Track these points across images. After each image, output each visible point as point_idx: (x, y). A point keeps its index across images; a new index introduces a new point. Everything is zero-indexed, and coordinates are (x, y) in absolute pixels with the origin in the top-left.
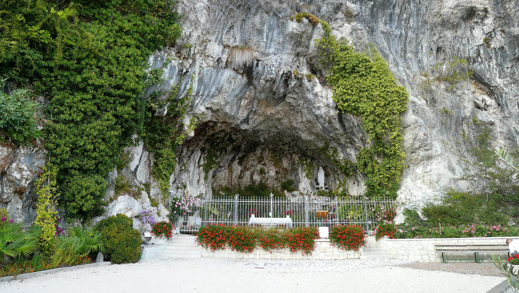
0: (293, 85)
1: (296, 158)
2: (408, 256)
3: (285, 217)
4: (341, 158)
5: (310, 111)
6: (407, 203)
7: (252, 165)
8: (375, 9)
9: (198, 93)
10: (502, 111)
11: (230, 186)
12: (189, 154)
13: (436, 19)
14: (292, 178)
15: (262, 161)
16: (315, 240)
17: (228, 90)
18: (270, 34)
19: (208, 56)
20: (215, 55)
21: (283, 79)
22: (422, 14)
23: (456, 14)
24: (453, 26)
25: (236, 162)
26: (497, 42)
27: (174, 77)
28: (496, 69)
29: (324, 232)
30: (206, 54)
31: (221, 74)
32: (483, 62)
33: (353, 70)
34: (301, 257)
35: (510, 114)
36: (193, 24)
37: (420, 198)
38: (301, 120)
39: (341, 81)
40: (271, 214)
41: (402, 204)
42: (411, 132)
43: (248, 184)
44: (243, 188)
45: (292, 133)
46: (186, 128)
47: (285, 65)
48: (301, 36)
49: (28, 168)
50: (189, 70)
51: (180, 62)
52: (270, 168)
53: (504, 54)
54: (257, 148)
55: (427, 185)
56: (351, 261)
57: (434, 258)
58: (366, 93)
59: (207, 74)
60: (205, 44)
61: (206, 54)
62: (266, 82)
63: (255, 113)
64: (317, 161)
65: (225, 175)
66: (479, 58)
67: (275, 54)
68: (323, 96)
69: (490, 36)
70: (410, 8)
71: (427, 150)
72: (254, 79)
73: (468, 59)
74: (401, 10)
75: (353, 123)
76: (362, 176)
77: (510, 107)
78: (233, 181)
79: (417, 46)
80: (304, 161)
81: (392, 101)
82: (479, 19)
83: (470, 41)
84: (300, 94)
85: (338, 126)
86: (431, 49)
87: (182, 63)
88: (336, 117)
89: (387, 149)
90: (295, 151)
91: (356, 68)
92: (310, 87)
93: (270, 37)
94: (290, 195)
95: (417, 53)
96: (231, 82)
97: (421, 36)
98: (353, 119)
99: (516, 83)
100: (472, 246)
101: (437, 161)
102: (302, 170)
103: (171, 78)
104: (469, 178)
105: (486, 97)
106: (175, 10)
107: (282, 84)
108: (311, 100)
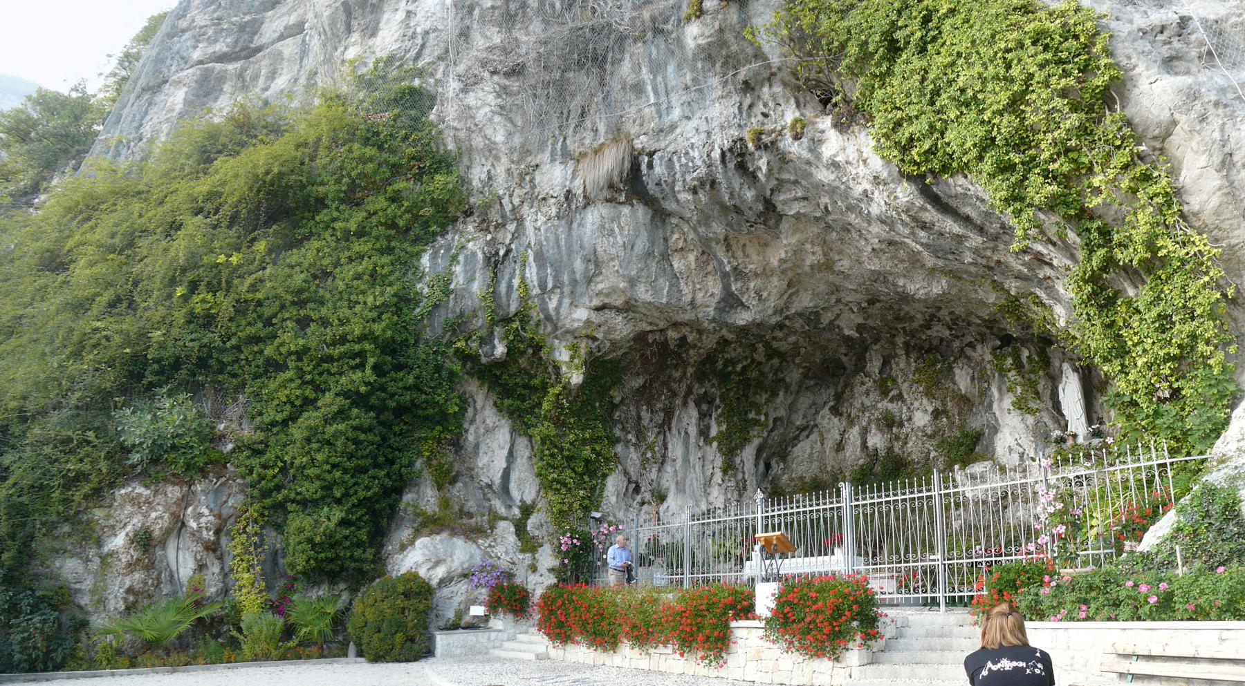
3: (833, 554)
9: (543, 286)
12: (660, 417)
16: (733, 624)
17: (613, 251)
19: (544, 199)
21: (731, 165)
27: (478, 275)
31: (580, 225)
33: (893, 49)
38: (869, 249)
42: (1194, 144)
48: (722, 43)
49: (211, 511)
50: (513, 246)
51: (489, 237)
52: (916, 404)
59: (547, 239)
60: (528, 178)
67: (688, 118)
72: (662, 202)
87: (493, 239)
88: (919, 202)
92: (806, 154)
93: (661, 88)
96: (612, 230)
102: (1000, 390)
103: (471, 280)
106: (442, 148)
107: (737, 181)
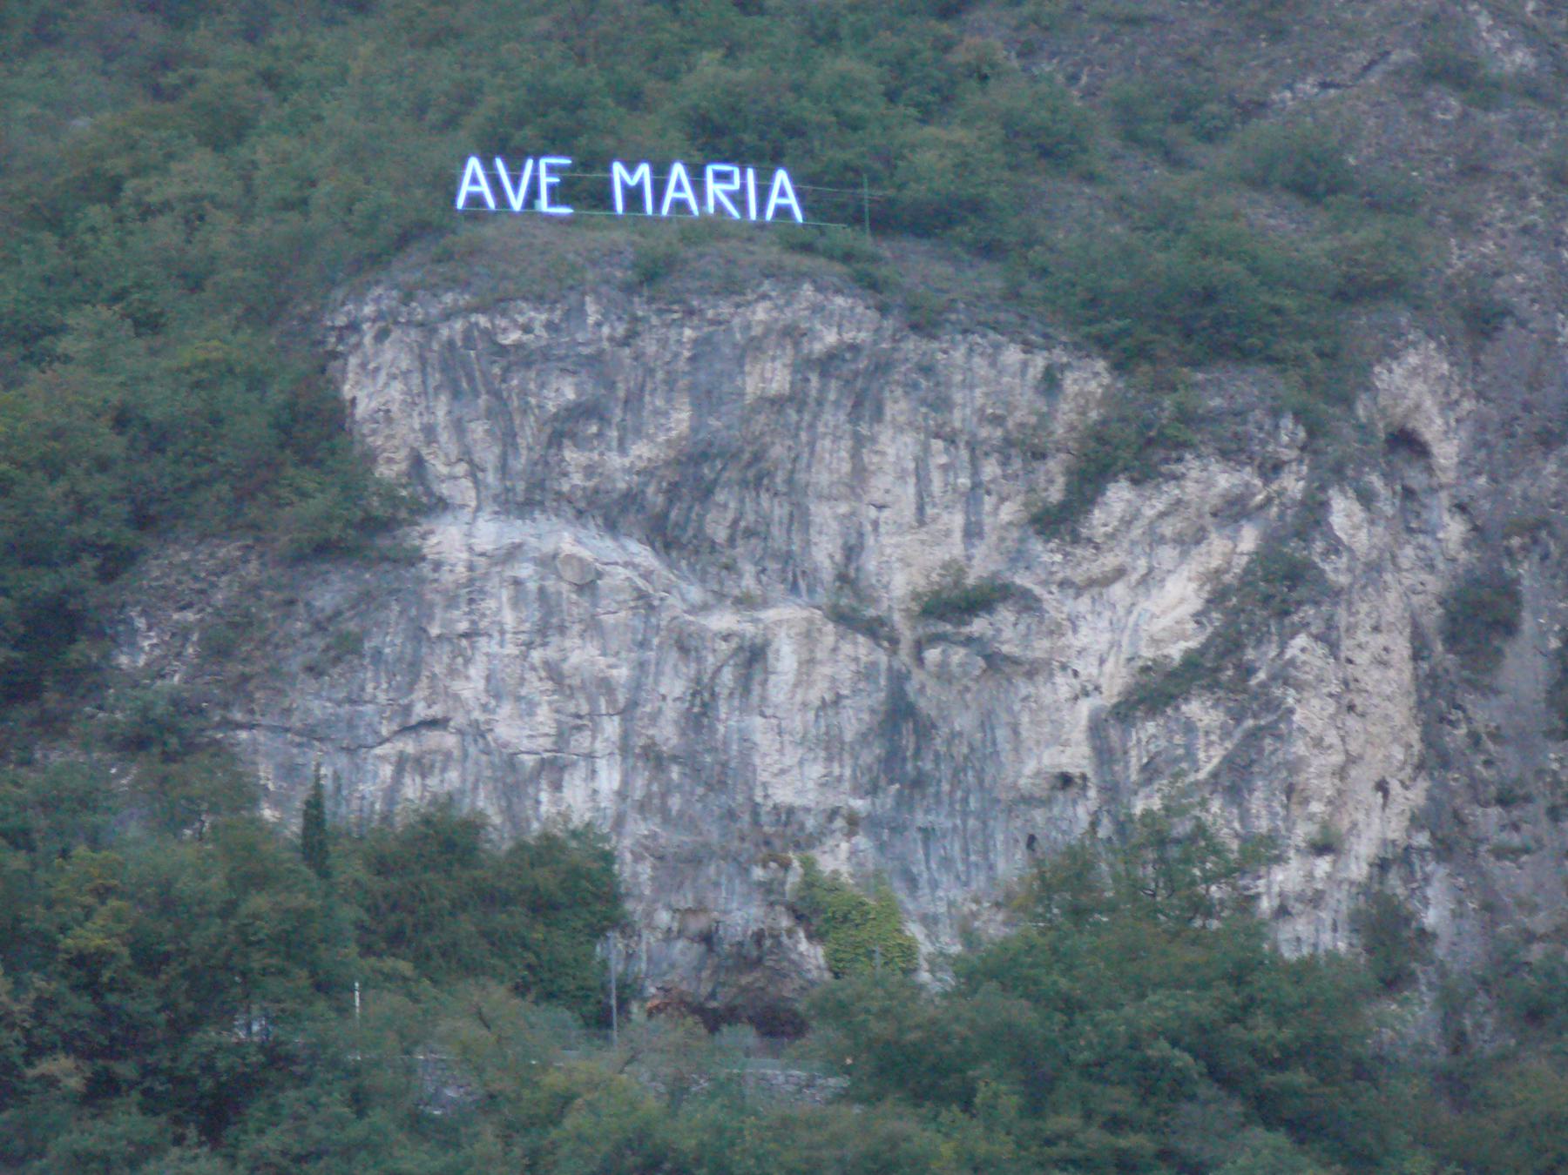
33: (845, 919)
39: (832, 935)
63: (723, 984)
79: (985, 843)
97: (991, 823)
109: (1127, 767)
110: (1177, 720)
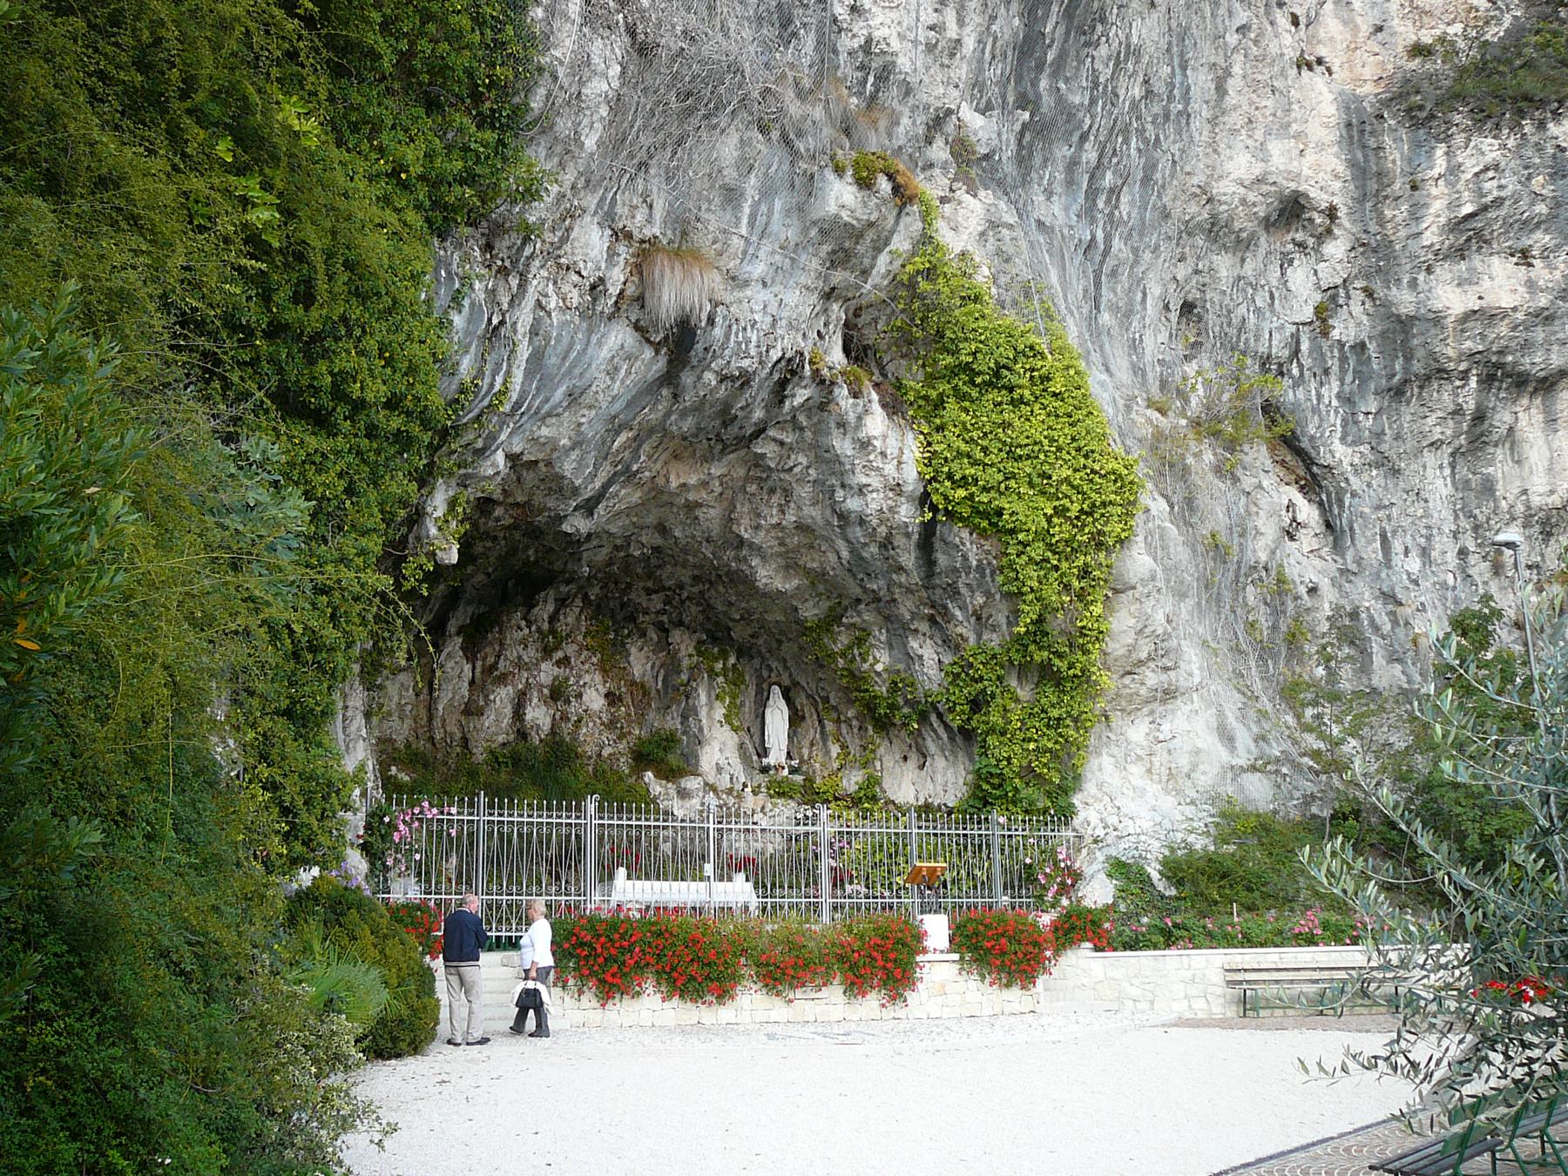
0: (798, 401)
1: (684, 645)
2: (1152, 1002)
3: (730, 879)
4: (879, 667)
5: (825, 493)
6: (1110, 840)
7: (520, 664)
8: (1028, 137)
10: (1337, 547)
11: (422, 745)
13: (1193, 209)
14: (673, 722)
15: (557, 648)
16: (919, 958)
18: (763, 208)
20: (590, 264)
21: (776, 376)
22: (1160, 182)
23: (1254, 205)
24: (1239, 241)
25: (455, 644)
26: (1351, 324)
28: (1336, 412)
29: (937, 928)
30: (563, 260)
32: (1304, 382)
34: (876, 1014)
35: (1359, 564)
36: (558, 149)
37: (1147, 825)
40: (709, 869)
41: (1096, 841)
42: (1133, 608)
43: (501, 739)
44: (479, 754)
45: (719, 558)
46: (433, 531)
47: (790, 326)
48: (858, 236)
52: (587, 678)
53: (1364, 369)
54: (543, 594)
55: (1160, 782)
56: (1012, 1019)
57: (1219, 1003)
58: (1027, 467)
61: (563, 260)
62: (721, 381)
64: (757, 662)
65: (401, 696)
66: (1295, 365)
68: (889, 452)
69: (1334, 298)
70: (1129, 155)
71: (1166, 669)
72: (688, 368)
73: (1265, 362)
74: (1100, 157)
75: (965, 558)
76: (945, 736)
77: (1361, 541)
78: (437, 723)
80: (716, 660)
81: (1104, 504)
82: (1311, 236)
83: (1277, 302)
84: (808, 434)
85: (908, 558)
86: (1167, 307)
88: (915, 530)
89: (1060, 656)
90: (687, 620)
91: (1005, 372)
93: (761, 220)
94: (673, 792)
95: (1129, 314)
96: (616, 369)
98: (968, 546)
99: (1383, 465)
100: (1314, 969)
101: (1188, 708)
104: (1269, 767)
105: (1299, 499)
107: (764, 394)
108: (842, 460)
109: (1415, 215)
110: (1539, 148)
